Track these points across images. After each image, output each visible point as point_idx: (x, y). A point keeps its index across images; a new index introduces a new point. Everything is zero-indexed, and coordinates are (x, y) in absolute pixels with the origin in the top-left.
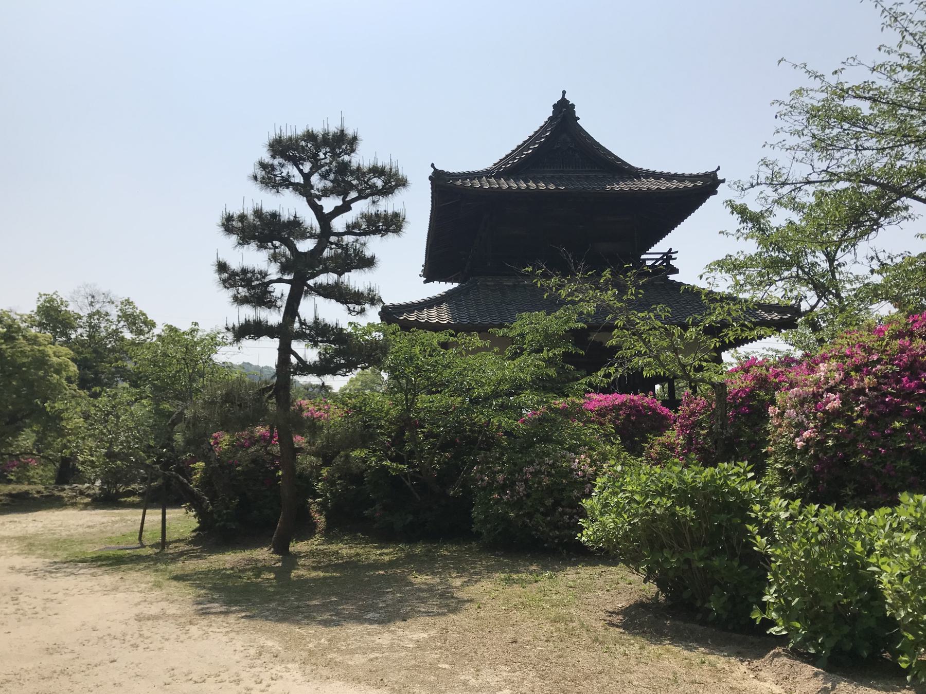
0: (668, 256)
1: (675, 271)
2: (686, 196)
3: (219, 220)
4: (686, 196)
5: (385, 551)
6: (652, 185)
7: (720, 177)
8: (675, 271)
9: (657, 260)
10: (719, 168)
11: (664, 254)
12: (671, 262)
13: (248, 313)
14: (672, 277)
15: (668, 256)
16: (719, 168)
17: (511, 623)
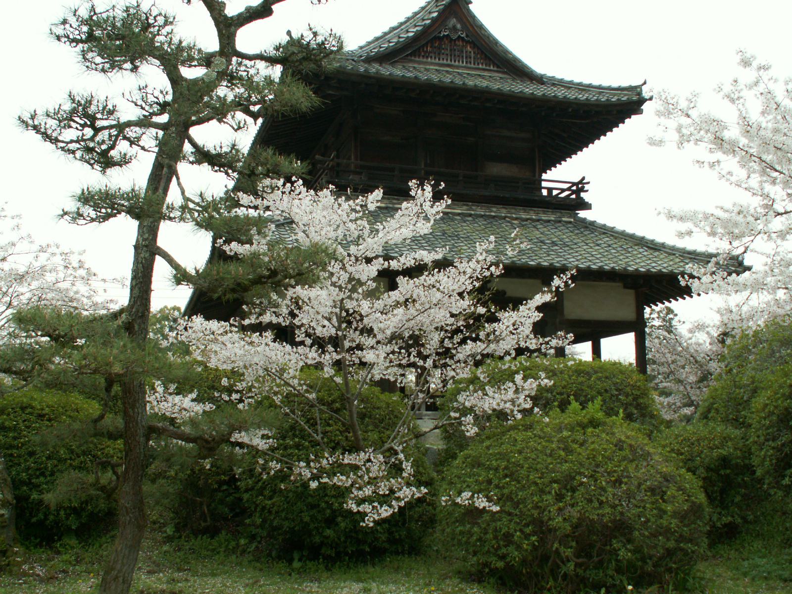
0: (579, 187)
1: (586, 206)
2: (598, 114)
3: (741, 68)
4: (598, 114)
5: (544, 217)
6: (561, 93)
7: (646, 94)
8: (586, 206)
9: (563, 190)
10: (645, 83)
11: (574, 184)
12: (583, 195)
13: (93, 178)
14: (582, 214)
15: (579, 187)
16: (645, 83)
17: (685, 121)
